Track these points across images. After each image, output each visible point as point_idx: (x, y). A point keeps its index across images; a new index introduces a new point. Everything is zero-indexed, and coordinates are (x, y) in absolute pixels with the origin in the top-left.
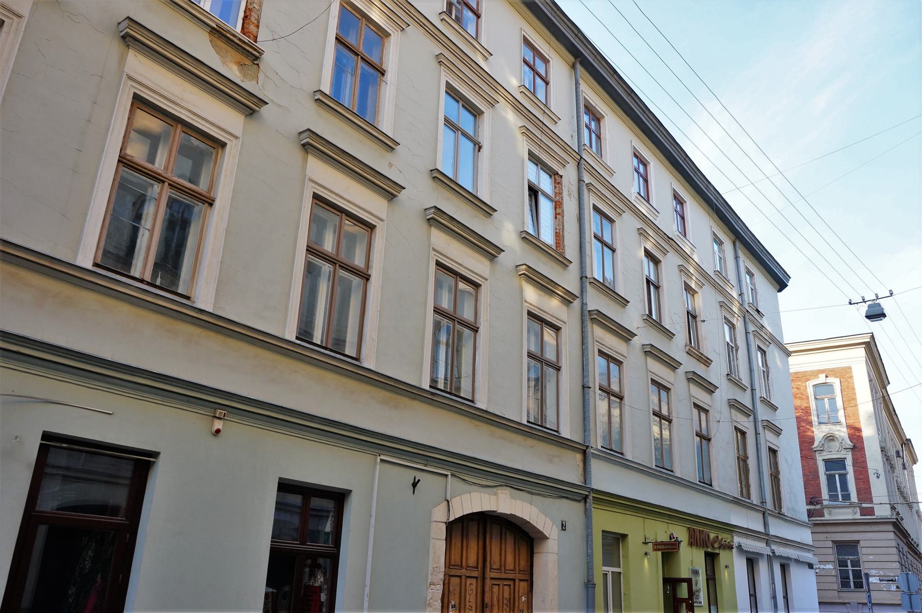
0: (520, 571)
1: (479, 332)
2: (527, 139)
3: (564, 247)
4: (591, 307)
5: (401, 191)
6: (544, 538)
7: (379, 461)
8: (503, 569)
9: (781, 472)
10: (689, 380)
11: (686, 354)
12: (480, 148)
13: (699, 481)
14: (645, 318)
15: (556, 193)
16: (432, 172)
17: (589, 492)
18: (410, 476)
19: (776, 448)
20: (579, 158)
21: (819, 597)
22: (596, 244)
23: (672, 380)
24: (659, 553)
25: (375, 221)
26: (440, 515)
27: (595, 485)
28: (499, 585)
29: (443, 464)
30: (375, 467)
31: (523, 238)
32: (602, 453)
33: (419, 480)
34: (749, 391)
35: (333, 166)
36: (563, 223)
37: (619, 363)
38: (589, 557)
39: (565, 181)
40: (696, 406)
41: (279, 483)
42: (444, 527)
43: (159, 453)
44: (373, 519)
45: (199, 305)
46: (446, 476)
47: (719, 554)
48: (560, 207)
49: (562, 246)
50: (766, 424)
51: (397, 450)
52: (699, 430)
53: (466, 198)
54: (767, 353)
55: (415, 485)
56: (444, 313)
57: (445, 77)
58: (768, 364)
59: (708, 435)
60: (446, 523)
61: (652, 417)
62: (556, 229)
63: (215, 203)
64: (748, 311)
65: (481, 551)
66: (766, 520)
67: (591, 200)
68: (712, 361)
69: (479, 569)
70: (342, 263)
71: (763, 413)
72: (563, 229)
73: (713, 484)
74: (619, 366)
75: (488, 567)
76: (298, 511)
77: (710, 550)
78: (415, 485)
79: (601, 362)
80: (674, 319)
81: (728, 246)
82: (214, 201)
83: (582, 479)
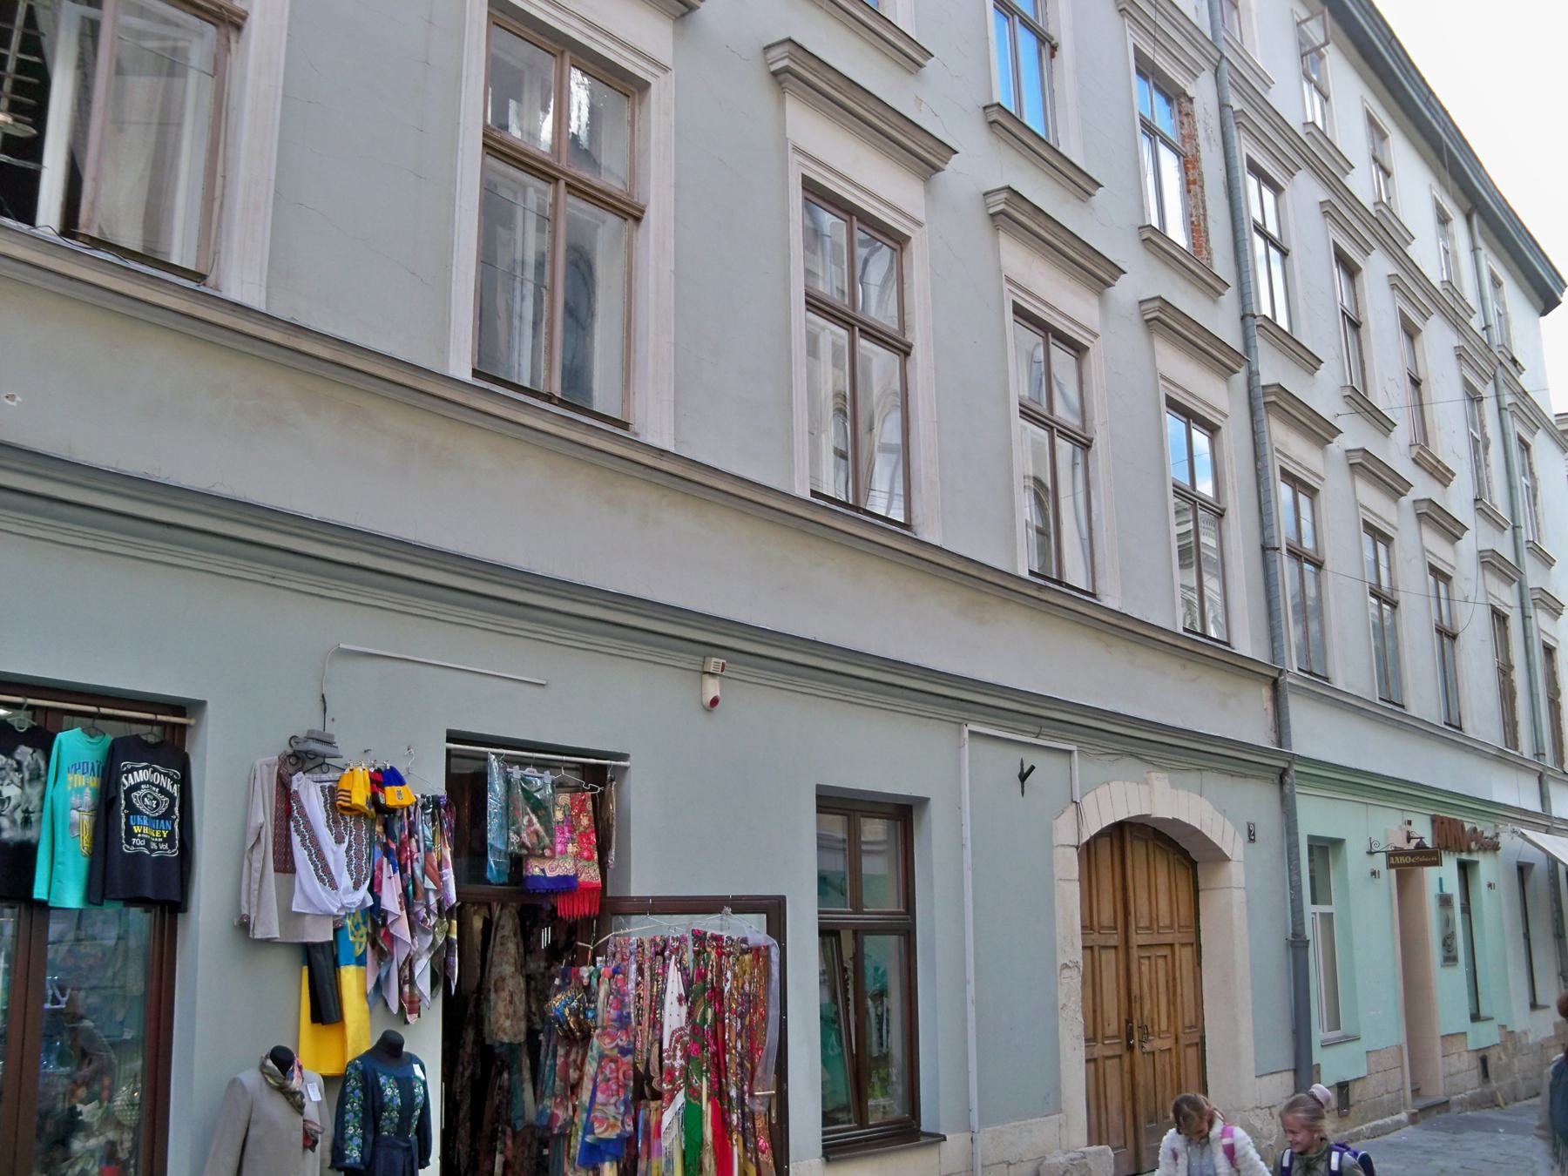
0: (1179, 926)
1: (1093, 448)
2: (1132, 25)
3: (1209, 253)
4: (1266, 378)
5: (949, 159)
6: (1219, 857)
7: (966, 735)
8: (1155, 926)
9: (1562, 691)
10: (1420, 517)
11: (1411, 462)
12: (1054, 48)
13: (1300, 669)
14: (1348, 393)
15: (1183, 137)
16: (987, 111)
17: (1289, 762)
18: (1010, 761)
19: (1553, 643)
20: (1217, 56)
21: (1083, 941)
22: (1259, 242)
23: (1393, 520)
24: (1393, 871)
25: (909, 228)
26: (1068, 834)
27: (1298, 749)
28: (1149, 958)
29: (1108, 740)
30: (961, 747)
31: (1144, 240)
32: (1301, 680)
33: (1032, 768)
34: (1509, 533)
35: (829, 116)
36: (1203, 202)
37: (1078, 350)
38: (1296, 888)
39: (1198, 107)
40: (1370, 528)
41: (818, 797)
42: (1073, 854)
43: (201, 705)
44: (968, 853)
45: (234, 294)
46: (1070, 752)
47: (1476, 863)
48: (1194, 168)
49: (1204, 252)
50: (1538, 596)
51: (926, 696)
52: (1294, 538)
53: (1052, 165)
54: (1532, 449)
55: (1023, 777)
56: (818, 304)
57: (1133, 38)
58: (1535, 470)
59: (1452, 629)
60: (1077, 847)
61: (1019, 423)
62: (1191, 216)
63: (645, 216)
64: (1501, 363)
65: (1119, 895)
66: (1544, 789)
67: (1245, 147)
68: (1454, 475)
69: (1119, 930)
70: (868, 325)
71: (1534, 576)
72: (1205, 215)
73: (1465, 725)
74: (1311, 498)
75: (1133, 922)
76: (841, 846)
77: (1464, 856)
78: (1023, 777)
79: (1285, 492)
80: (1389, 394)
81: (1458, 224)
82: (643, 212)
83: (1273, 736)
